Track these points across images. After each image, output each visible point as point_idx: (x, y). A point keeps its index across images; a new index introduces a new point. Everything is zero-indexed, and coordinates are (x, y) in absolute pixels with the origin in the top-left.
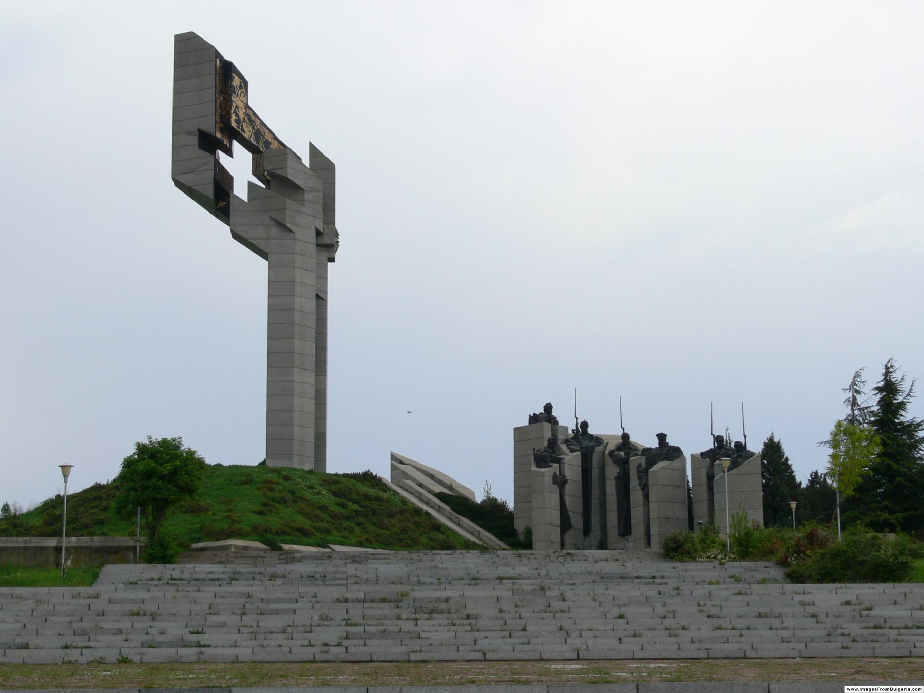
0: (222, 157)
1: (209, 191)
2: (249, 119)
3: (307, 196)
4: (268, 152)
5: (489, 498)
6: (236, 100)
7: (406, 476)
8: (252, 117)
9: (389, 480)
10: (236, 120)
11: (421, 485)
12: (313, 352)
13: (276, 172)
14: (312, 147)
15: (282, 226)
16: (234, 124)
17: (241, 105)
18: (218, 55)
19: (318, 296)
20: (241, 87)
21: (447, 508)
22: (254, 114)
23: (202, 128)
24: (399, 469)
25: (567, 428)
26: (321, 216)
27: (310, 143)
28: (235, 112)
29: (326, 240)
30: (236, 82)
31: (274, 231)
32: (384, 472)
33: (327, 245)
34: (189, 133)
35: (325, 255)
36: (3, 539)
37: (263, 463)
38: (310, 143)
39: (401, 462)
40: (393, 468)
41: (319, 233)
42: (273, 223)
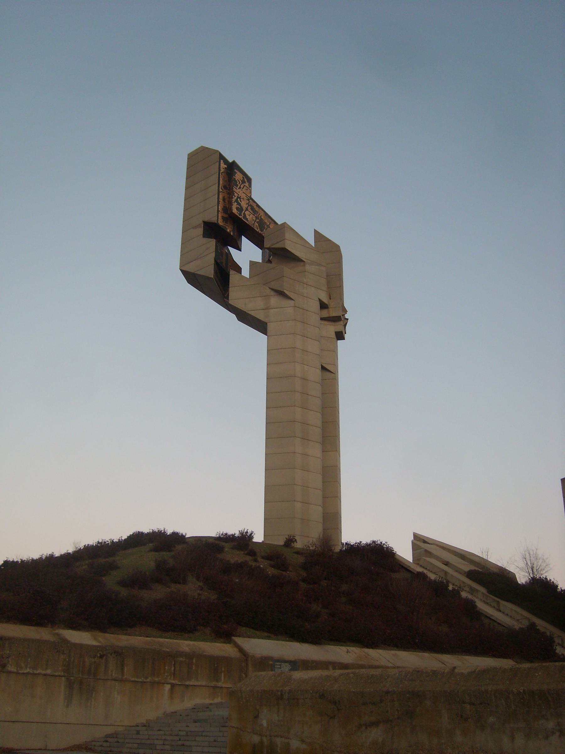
0: (232, 250)
1: (209, 271)
2: (252, 209)
3: (308, 267)
4: (280, 253)
5: (533, 579)
6: (238, 192)
7: (428, 553)
8: (255, 208)
9: (411, 560)
10: (237, 208)
11: (447, 564)
12: (319, 424)
13: (274, 246)
14: (316, 232)
15: (281, 294)
16: (235, 211)
17: (244, 196)
18: (222, 157)
19: (323, 368)
20: (243, 182)
21: (482, 589)
22: (258, 206)
23: (206, 219)
24: (421, 548)
25: (557, 586)
26: (325, 288)
27: (315, 230)
28: (236, 201)
29: (333, 313)
30: (238, 176)
31: (275, 300)
32: (404, 552)
33: (335, 319)
34: (195, 228)
35: (331, 329)
36: (5, 625)
37: (263, 542)
38: (315, 230)
39: (425, 542)
40: (415, 547)
41: (323, 306)
42: (272, 293)
